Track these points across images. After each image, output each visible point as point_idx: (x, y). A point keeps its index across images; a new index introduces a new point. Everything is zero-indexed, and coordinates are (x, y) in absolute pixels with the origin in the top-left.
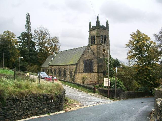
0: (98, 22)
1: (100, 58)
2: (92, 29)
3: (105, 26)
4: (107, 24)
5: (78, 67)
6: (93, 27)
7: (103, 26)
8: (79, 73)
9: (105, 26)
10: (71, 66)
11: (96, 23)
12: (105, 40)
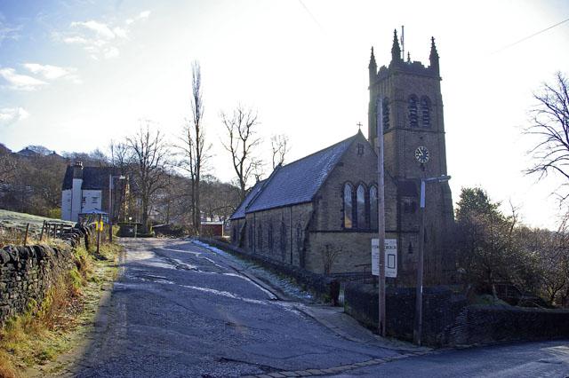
0: (409, 59)
1: (408, 177)
2: (378, 78)
3: (426, 63)
4: (434, 57)
5: (321, 211)
6: (383, 68)
7: (418, 64)
8: (324, 232)
9: (426, 63)
10: (299, 207)
11: (391, 55)
12: (424, 112)
